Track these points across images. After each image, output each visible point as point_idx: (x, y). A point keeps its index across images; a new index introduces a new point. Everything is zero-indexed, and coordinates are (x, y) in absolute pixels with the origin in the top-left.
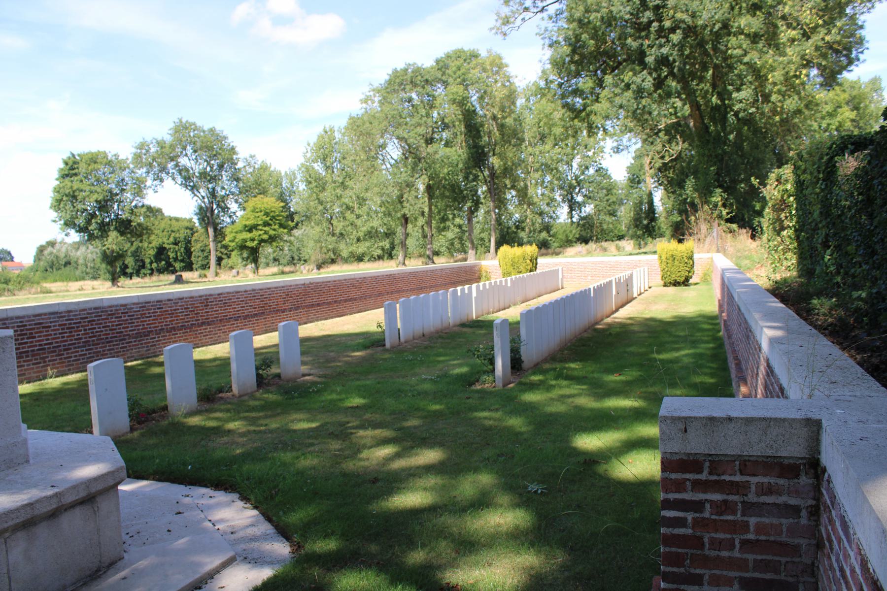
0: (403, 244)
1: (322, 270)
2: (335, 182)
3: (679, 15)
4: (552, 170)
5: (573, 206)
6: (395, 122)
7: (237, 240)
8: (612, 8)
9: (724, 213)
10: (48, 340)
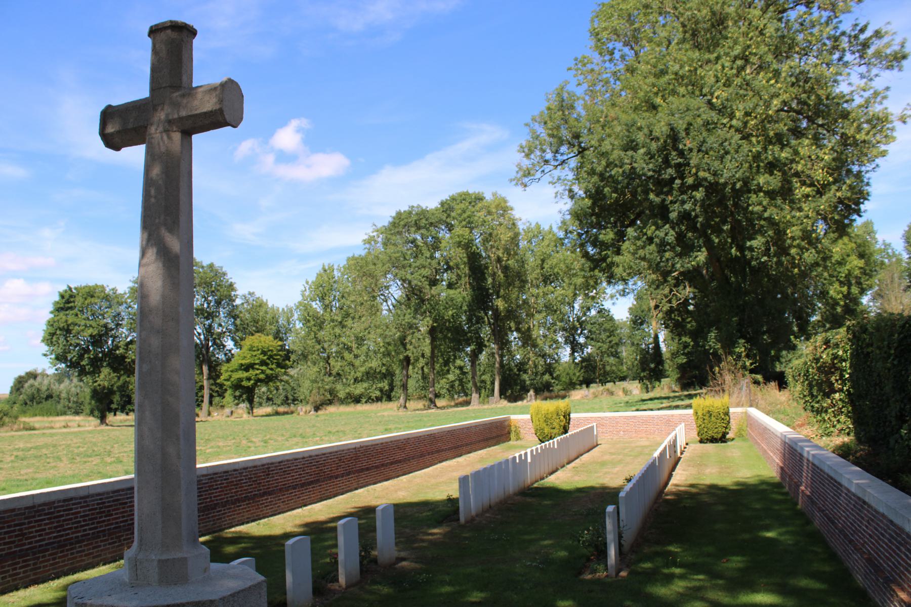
0: (405, 387)
1: (320, 412)
2: (333, 321)
3: (701, 174)
4: (556, 311)
5: (575, 347)
6: (397, 264)
7: (232, 379)
8: (635, 165)
9: (748, 364)
10: (123, 517)
